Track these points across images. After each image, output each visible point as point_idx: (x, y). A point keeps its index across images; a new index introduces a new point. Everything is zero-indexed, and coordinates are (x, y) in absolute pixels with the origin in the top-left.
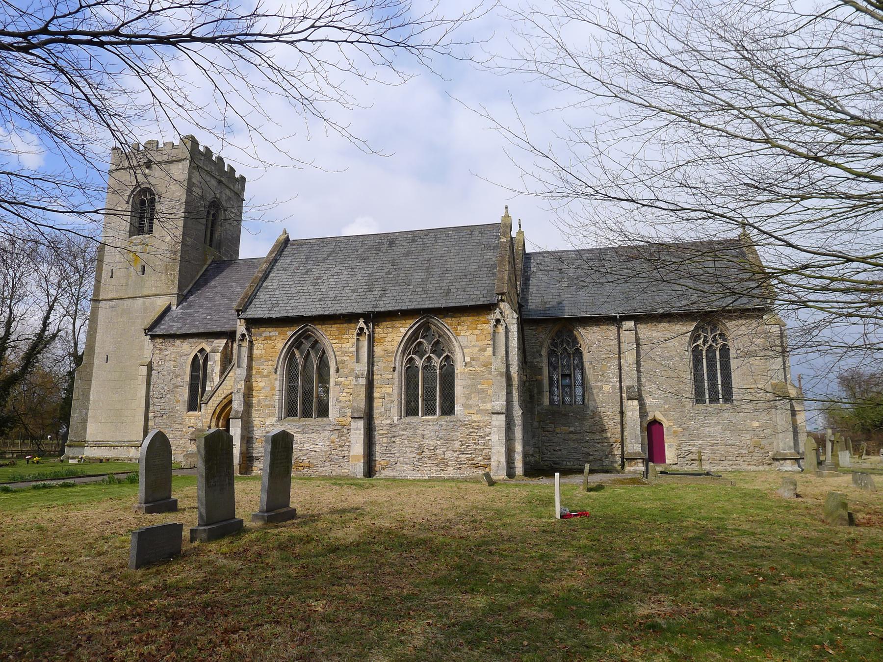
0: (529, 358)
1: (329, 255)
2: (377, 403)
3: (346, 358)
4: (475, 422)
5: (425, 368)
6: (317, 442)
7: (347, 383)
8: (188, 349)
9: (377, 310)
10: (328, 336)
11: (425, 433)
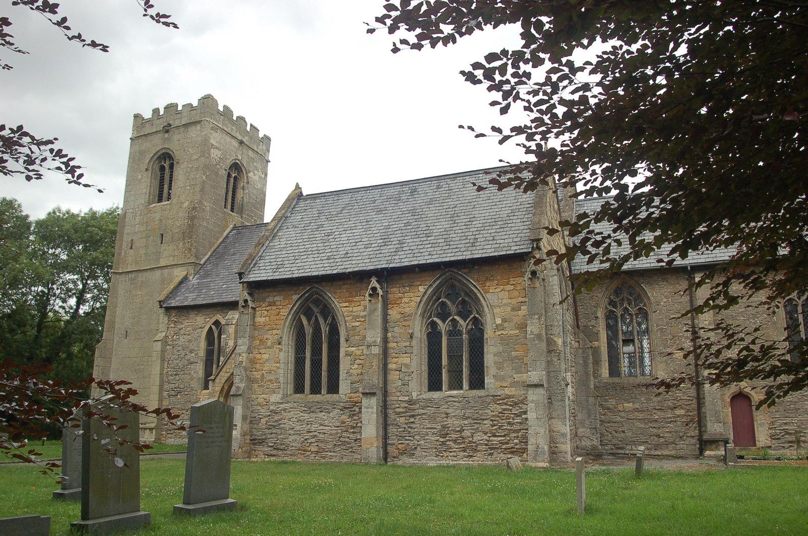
0: (582, 322)
1: (343, 209)
2: (393, 376)
3: (357, 324)
4: (509, 397)
5: (450, 334)
6: (326, 423)
7: (358, 353)
8: (203, 322)
9: (391, 266)
10: (473, 282)
11: (449, 411)
